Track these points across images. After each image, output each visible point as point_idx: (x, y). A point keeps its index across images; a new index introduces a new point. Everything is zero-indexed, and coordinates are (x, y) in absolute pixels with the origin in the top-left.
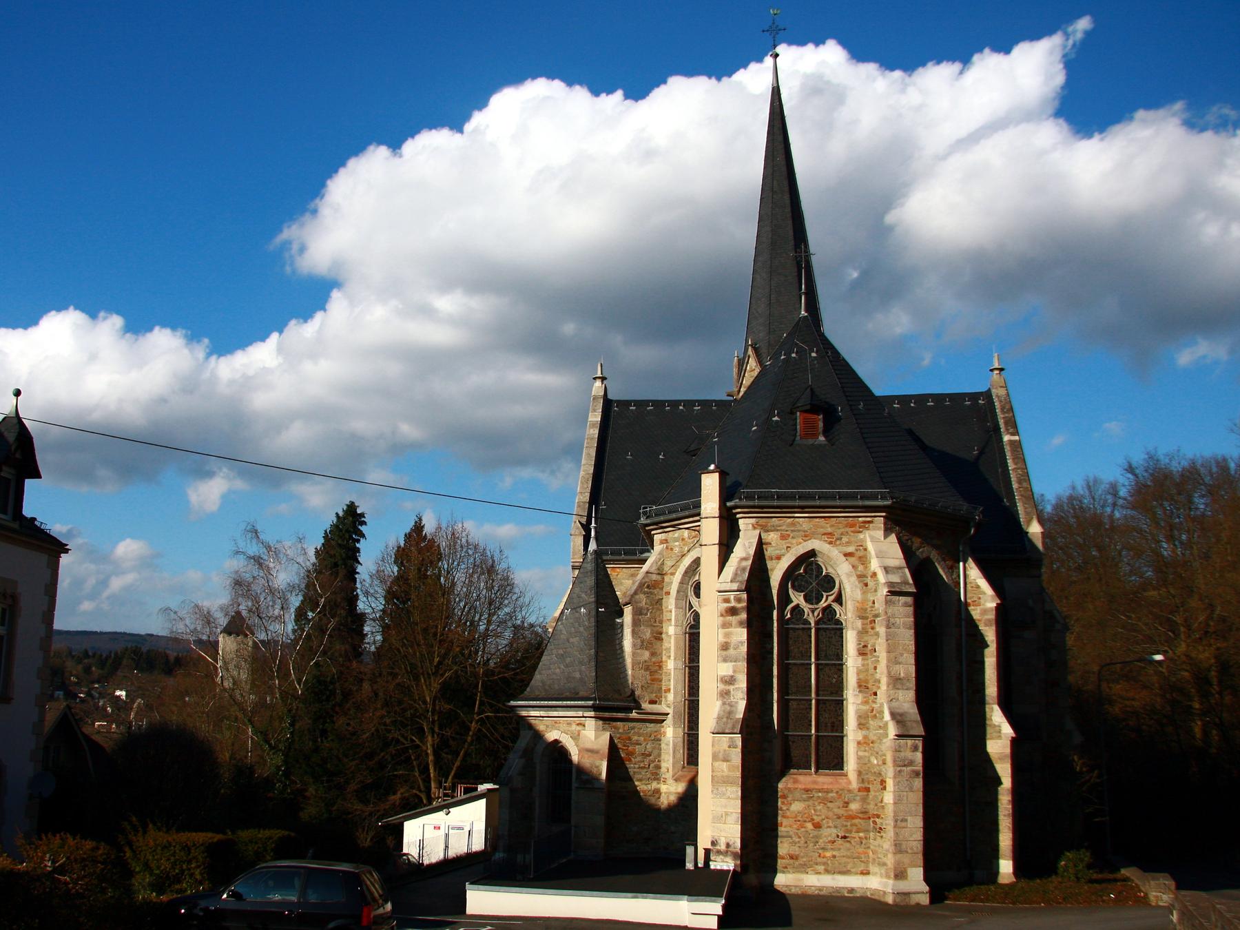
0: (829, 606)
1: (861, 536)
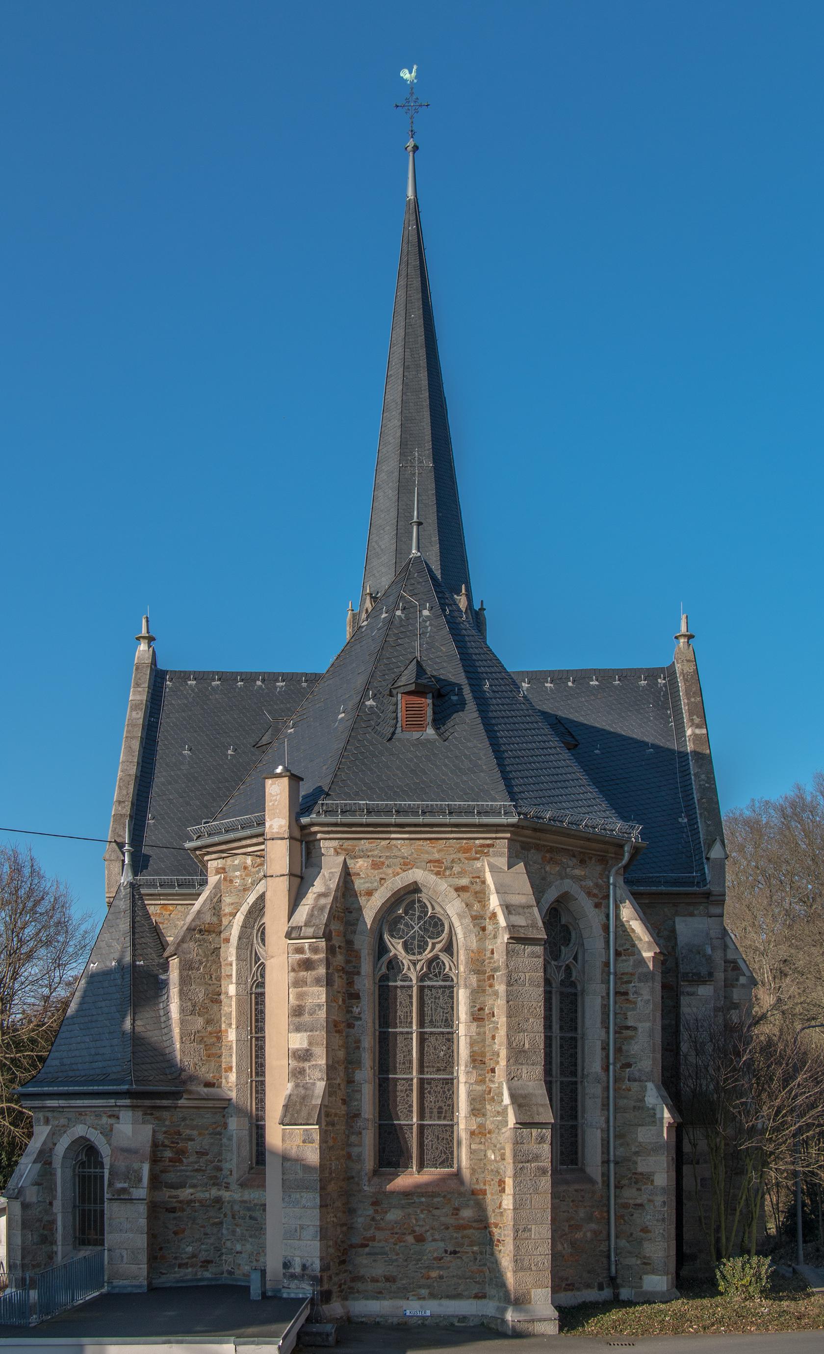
0: (436, 957)
1: (478, 864)
